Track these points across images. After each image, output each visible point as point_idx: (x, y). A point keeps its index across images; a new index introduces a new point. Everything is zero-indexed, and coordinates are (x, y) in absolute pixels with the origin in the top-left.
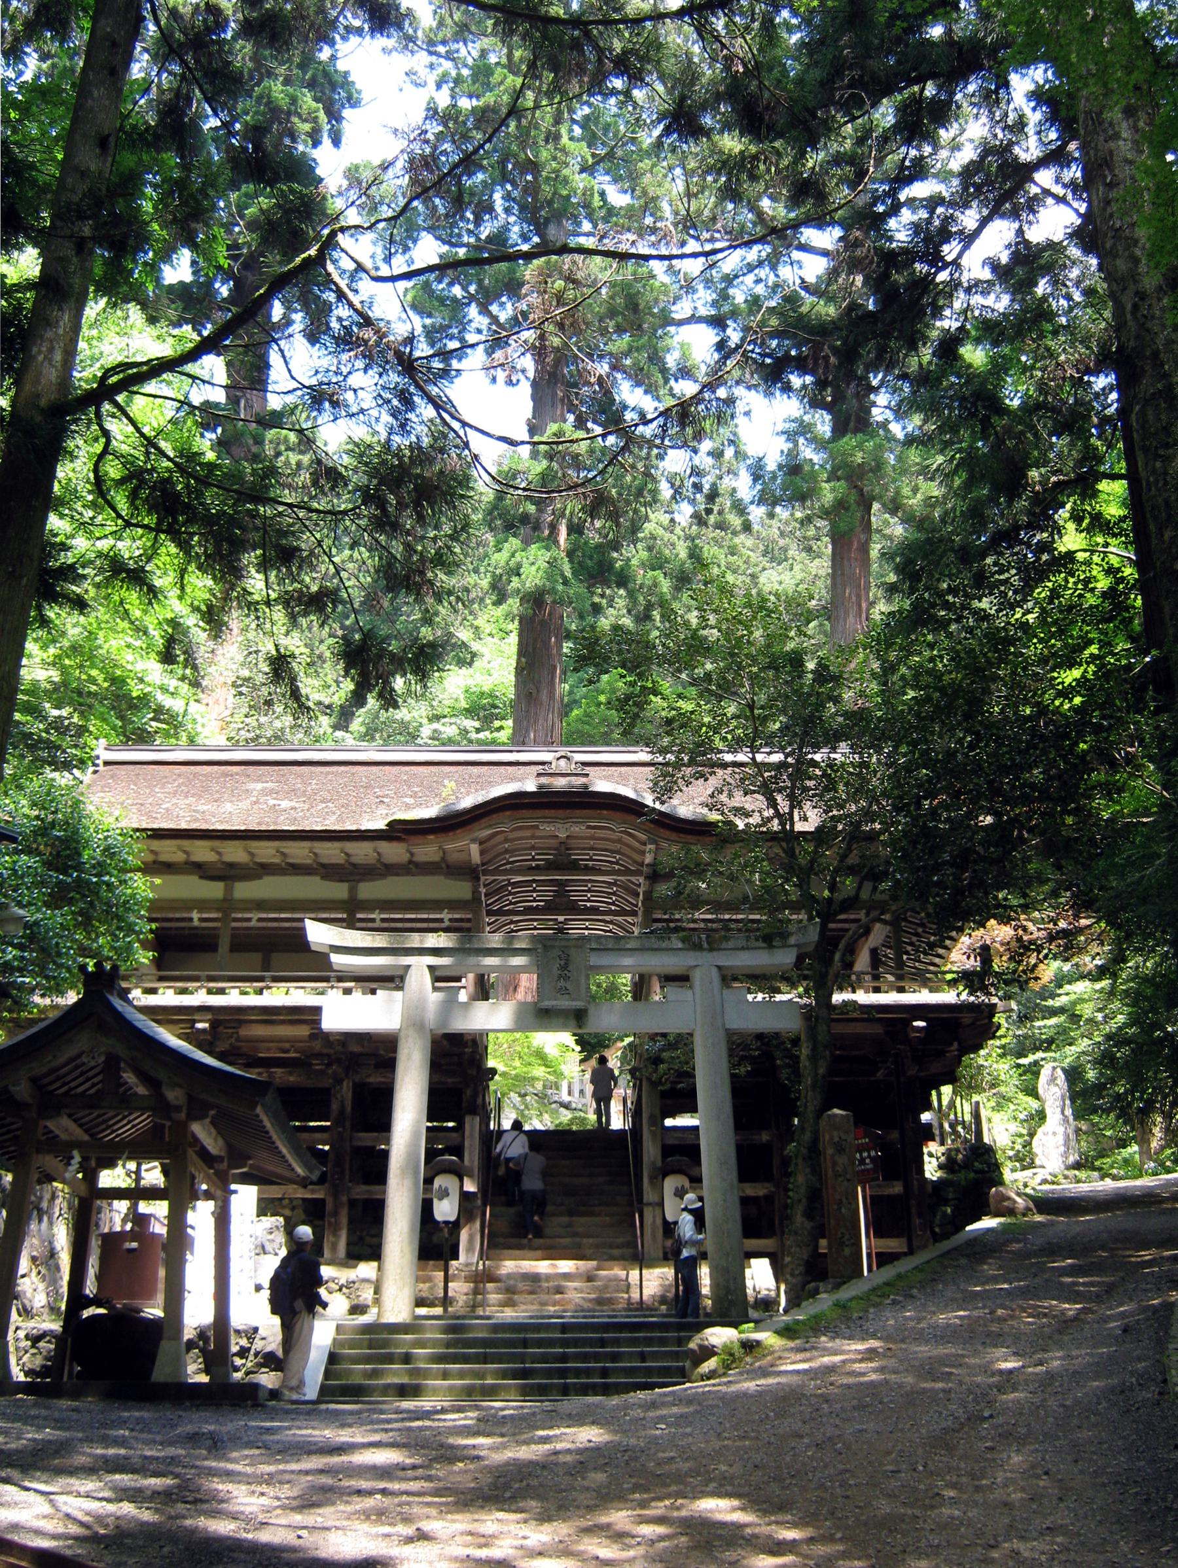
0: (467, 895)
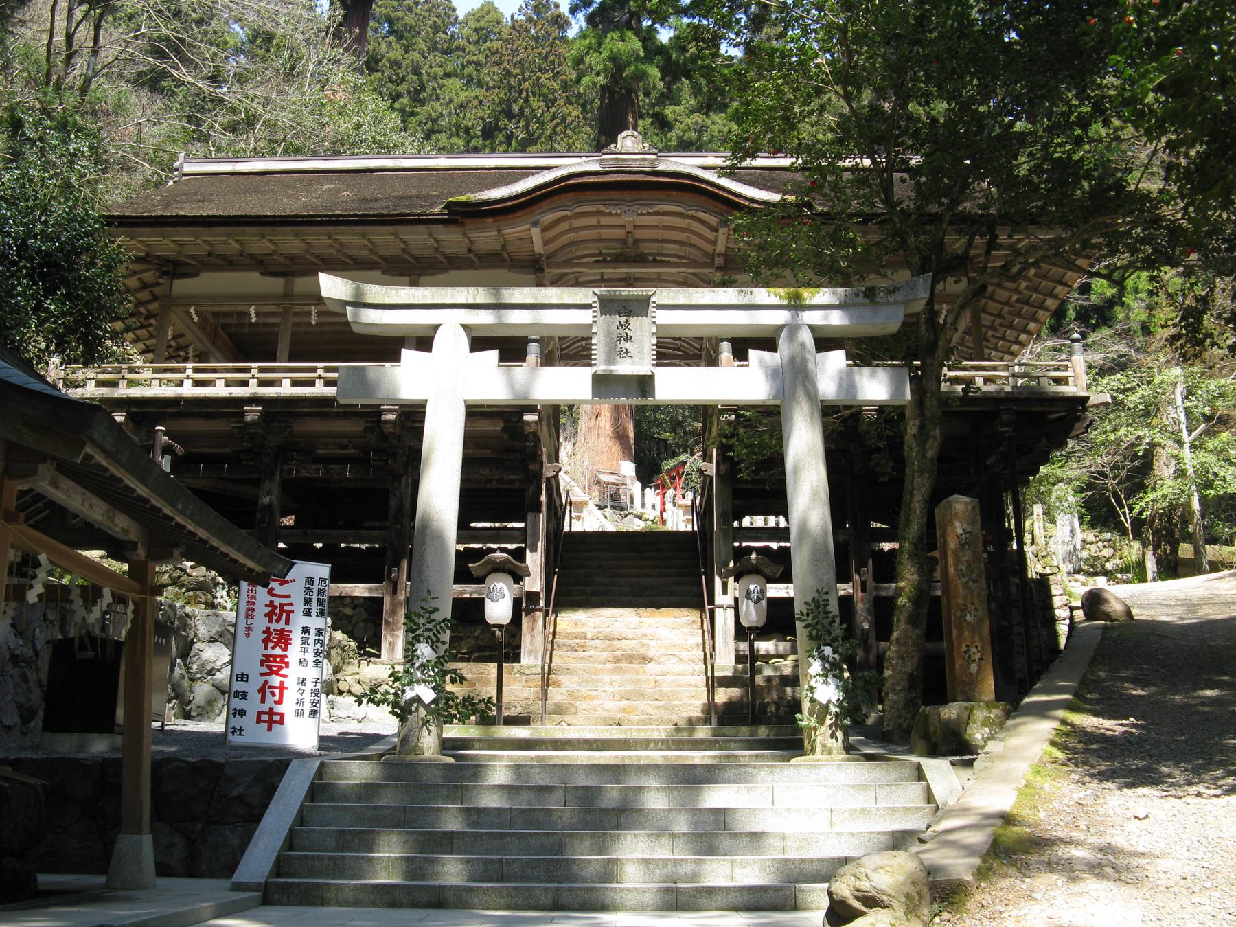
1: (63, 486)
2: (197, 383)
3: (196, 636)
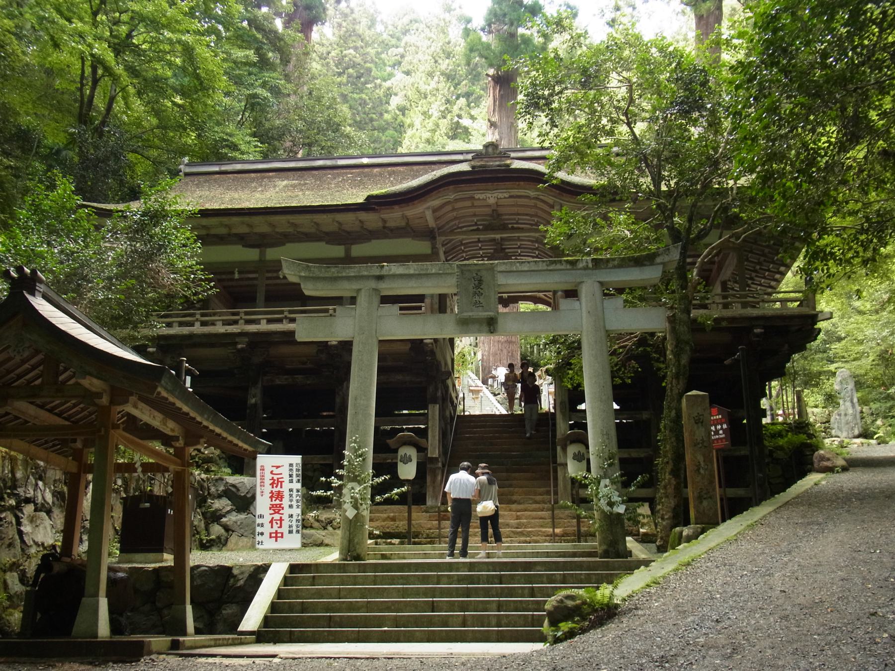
0: (429, 251)
1: (140, 407)
2: (204, 324)
3: (209, 493)
